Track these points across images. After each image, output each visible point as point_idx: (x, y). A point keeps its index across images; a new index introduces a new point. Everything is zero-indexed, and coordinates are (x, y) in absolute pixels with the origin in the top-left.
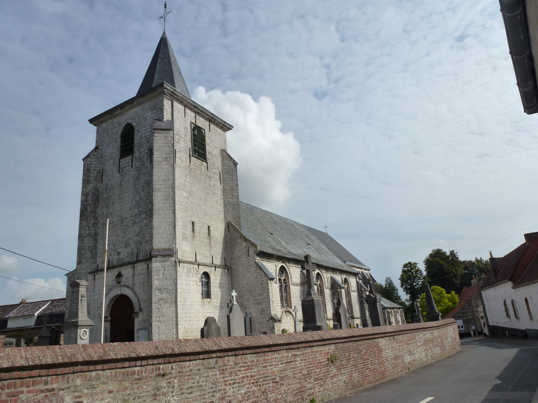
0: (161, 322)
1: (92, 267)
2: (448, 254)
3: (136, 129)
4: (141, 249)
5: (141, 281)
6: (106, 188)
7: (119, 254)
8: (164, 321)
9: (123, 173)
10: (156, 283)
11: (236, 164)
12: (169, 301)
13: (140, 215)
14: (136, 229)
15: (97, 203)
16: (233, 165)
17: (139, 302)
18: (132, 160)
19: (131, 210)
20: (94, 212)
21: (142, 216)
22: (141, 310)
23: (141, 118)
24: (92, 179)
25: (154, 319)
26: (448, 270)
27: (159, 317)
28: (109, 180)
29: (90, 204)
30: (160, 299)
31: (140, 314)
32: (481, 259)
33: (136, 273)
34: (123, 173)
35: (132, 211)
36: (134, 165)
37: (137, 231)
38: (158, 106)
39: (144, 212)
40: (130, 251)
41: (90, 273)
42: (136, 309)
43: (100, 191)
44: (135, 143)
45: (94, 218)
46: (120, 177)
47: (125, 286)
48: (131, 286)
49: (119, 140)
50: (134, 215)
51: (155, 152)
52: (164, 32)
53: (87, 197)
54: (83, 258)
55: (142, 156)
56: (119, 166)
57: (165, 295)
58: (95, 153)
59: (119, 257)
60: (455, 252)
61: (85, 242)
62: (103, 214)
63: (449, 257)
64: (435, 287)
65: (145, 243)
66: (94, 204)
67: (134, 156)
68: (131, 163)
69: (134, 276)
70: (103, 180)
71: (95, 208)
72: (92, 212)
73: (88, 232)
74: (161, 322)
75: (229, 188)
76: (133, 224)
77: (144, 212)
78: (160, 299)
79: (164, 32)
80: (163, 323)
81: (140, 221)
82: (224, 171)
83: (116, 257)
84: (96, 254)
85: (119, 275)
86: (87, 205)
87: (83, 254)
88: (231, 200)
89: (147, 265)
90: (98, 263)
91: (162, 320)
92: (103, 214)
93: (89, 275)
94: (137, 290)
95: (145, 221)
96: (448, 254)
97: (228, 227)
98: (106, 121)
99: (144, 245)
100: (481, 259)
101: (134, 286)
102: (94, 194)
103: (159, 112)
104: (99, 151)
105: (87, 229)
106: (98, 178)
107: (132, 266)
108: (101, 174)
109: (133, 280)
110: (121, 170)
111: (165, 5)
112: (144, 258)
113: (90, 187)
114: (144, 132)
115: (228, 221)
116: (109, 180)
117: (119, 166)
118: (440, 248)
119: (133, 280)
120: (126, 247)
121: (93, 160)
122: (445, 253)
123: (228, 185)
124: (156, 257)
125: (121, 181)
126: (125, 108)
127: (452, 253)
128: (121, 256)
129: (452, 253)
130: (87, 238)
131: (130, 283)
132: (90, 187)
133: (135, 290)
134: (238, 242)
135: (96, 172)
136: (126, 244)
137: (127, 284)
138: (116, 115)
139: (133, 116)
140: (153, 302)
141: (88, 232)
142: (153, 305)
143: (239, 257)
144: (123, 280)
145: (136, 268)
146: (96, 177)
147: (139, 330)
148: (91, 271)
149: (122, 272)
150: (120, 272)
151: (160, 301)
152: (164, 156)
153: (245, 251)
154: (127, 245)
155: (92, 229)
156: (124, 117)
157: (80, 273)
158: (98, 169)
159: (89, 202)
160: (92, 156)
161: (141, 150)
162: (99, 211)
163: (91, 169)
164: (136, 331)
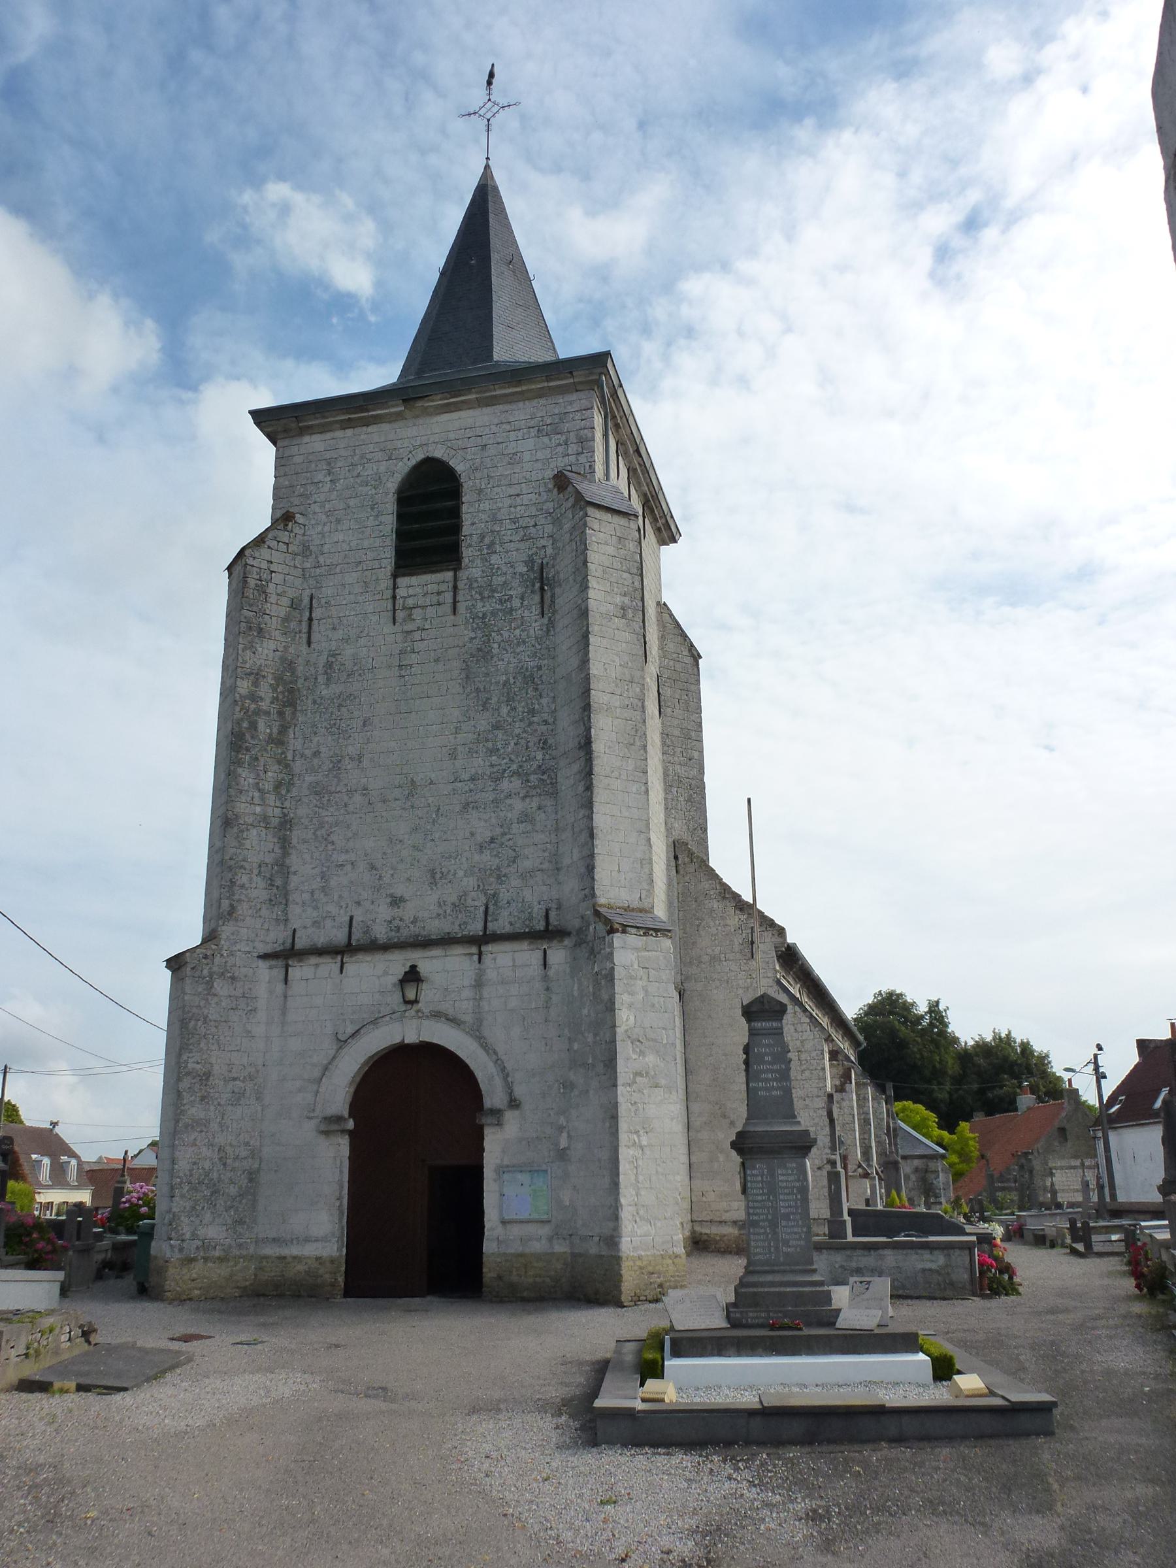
0: (642, 1148)
1: (272, 936)
2: (922, 1008)
3: (467, 485)
4: (504, 896)
5: (513, 1003)
6: (329, 665)
7: (396, 901)
8: (650, 1145)
9: (410, 626)
10: (625, 1018)
11: (696, 657)
12: (663, 1082)
13: (497, 779)
14: (481, 825)
15: (288, 711)
16: (689, 660)
17: (506, 1076)
18: (455, 587)
19: (453, 755)
20: (279, 741)
21: (505, 785)
22: (514, 1104)
23: (492, 450)
24: (273, 624)
25: (623, 1137)
26: (922, 1057)
27: (637, 1132)
28: (346, 641)
29: (268, 713)
30: (638, 1074)
31: (510, 1116)
32: (1008, 1036)
33: (491, 975)
34: (410, 626)
35: (459, 763)
36: (461, 607)
37: (483, 834)
38: (566, 426)
39: (516, 773)
40: (453, 898)
41: (265, 957)
42: (493, 1097)
43: (300, 669)
44: (465, 530)
45: (279, 762)
46: (400, 638)
47: (436, 1015)
48: (468, 1018)
49: (390, 506)
50: (466, 776)
51: (593, 582)
52: (487, 167)
53: (256, 684)
54: (239, 901)
55: (498, 580)
56: (394, 597)
57: (651, 1059)
58: (284, 536)
59: (397, 912)
60: (941, 1007)
61: (248, 844)
62: (317, 754)
63: (922, 1017)
64: (908, 1104)
65: (522, 877)
66: (281, 714)
67: (460, 574)
68: (448, 597)
69: (479, 984)
70: (315, 637)
71: (283, 730)
72: (271, 740)
73: (258, 809)
74: (642, 1148)
75: (677, 732)
76: (466, 806)
77: (516, 773)
78: (638, 1074)
79: (487, 167)
80: (648, 1152)
81: (496, 802)
82: (666, 674)
83: (384, 912)
84: (285, 893)
85: (412, 976)
86: (257, 712)
87: (242, 886)
88: (682, 771)
89: (540, 954)
90: (295, 923)
91: (644, 1143)
92: (317, 754)
93: (261, 963)
94: (496, 1034)
95: (519, 805)
96: (922, 1008)
97: (676, 858)
98: (324, 429)
99: (515, 882)
100: (1008, 1036)
101: (479, 1021)
102: (279, 679)
103: (573, 449)
104: (297, 530)
105: (256, 801)
106: (293, 625)
107: (474, 950)
108: (305, 615)
109: (478, 1000)
110: (400, 615)
111: (491, 75)
112: (519, 928)
113: (266, 652)
114: (508, 502)
115: (676, 835)
116: (346, 641)
117: (394, 597)
118: (892, 988)
119: (478, 1000)
120: (433, 883)
121: (276, 557)
122: (913, 1004)
123: (676, 722)
124: (624, 932)
125: (403, 652)
126: (419, 404)
127: (934, 1007)
128: (408, 911)
129: (934, 1007)
130: (254, 832)
131: (464, 1007)
132: (266, 652)
133: (486, 1032)
134: (712, 910)
135: (285, 601)
136: (432, 872)
137: (446, 1007)
138: (377, 420)
139: (452, 436)
140: (620, 1081)
141: (258, 809)
142: (620, 1088)
143: (714, 959)
144: (428, 995)
145: (487, 959)
146: (286, 619)
147: (501, 1170)
148: (268, 949)
149: (424, 968)
150: (413, 967)
151: (638, 1079)
152: (618, 600)
153: (738, 940)
154: (434, 877)
155: (271, 799)
156: (411, 431)
157: (232, 954)
158: (291, 593)
159: (264, 705)
160: (273, 544)
161: (494, 559)
162: (294, 741)
163: (271, 588)
164: (488, 1173)
